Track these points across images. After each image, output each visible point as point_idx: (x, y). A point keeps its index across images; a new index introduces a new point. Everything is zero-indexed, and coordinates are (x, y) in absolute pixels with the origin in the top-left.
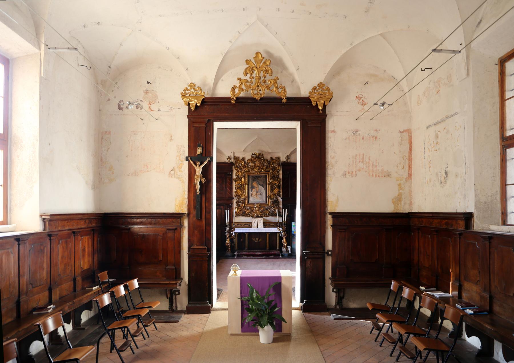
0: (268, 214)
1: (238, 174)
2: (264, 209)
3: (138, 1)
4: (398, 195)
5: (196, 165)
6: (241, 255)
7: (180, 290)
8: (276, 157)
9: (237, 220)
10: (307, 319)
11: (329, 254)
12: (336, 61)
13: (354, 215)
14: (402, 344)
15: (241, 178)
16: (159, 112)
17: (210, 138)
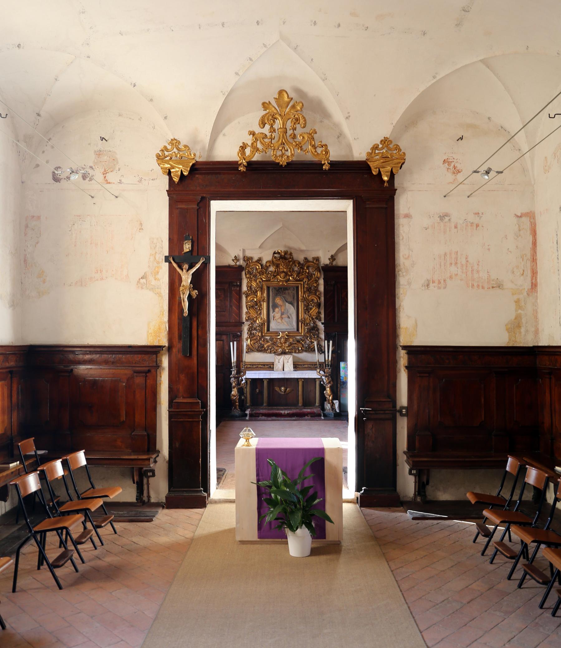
0: (300, 349)
1: (251, 285)
2: (293, 341)
3: (84, 11)
4: (516, 318)
5: (182, 270)
6: (258, 415)
7: (154, 470)
8: (313, 258)
9: (248, 358)
10: (368, 518)
11: (403, 413)
12: (409, 104)
13: (443, 349)
14: (528, 559)
15: (257, 292)
16: (120, 185)
17: (206, 226)
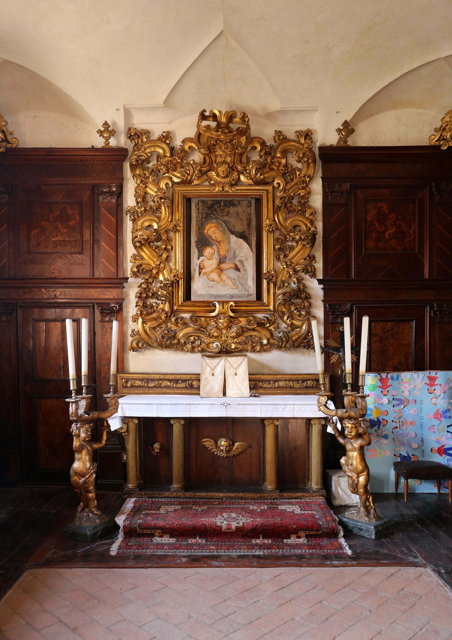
0: (265, 342)
8: (297, 132)
15: (159, 208)
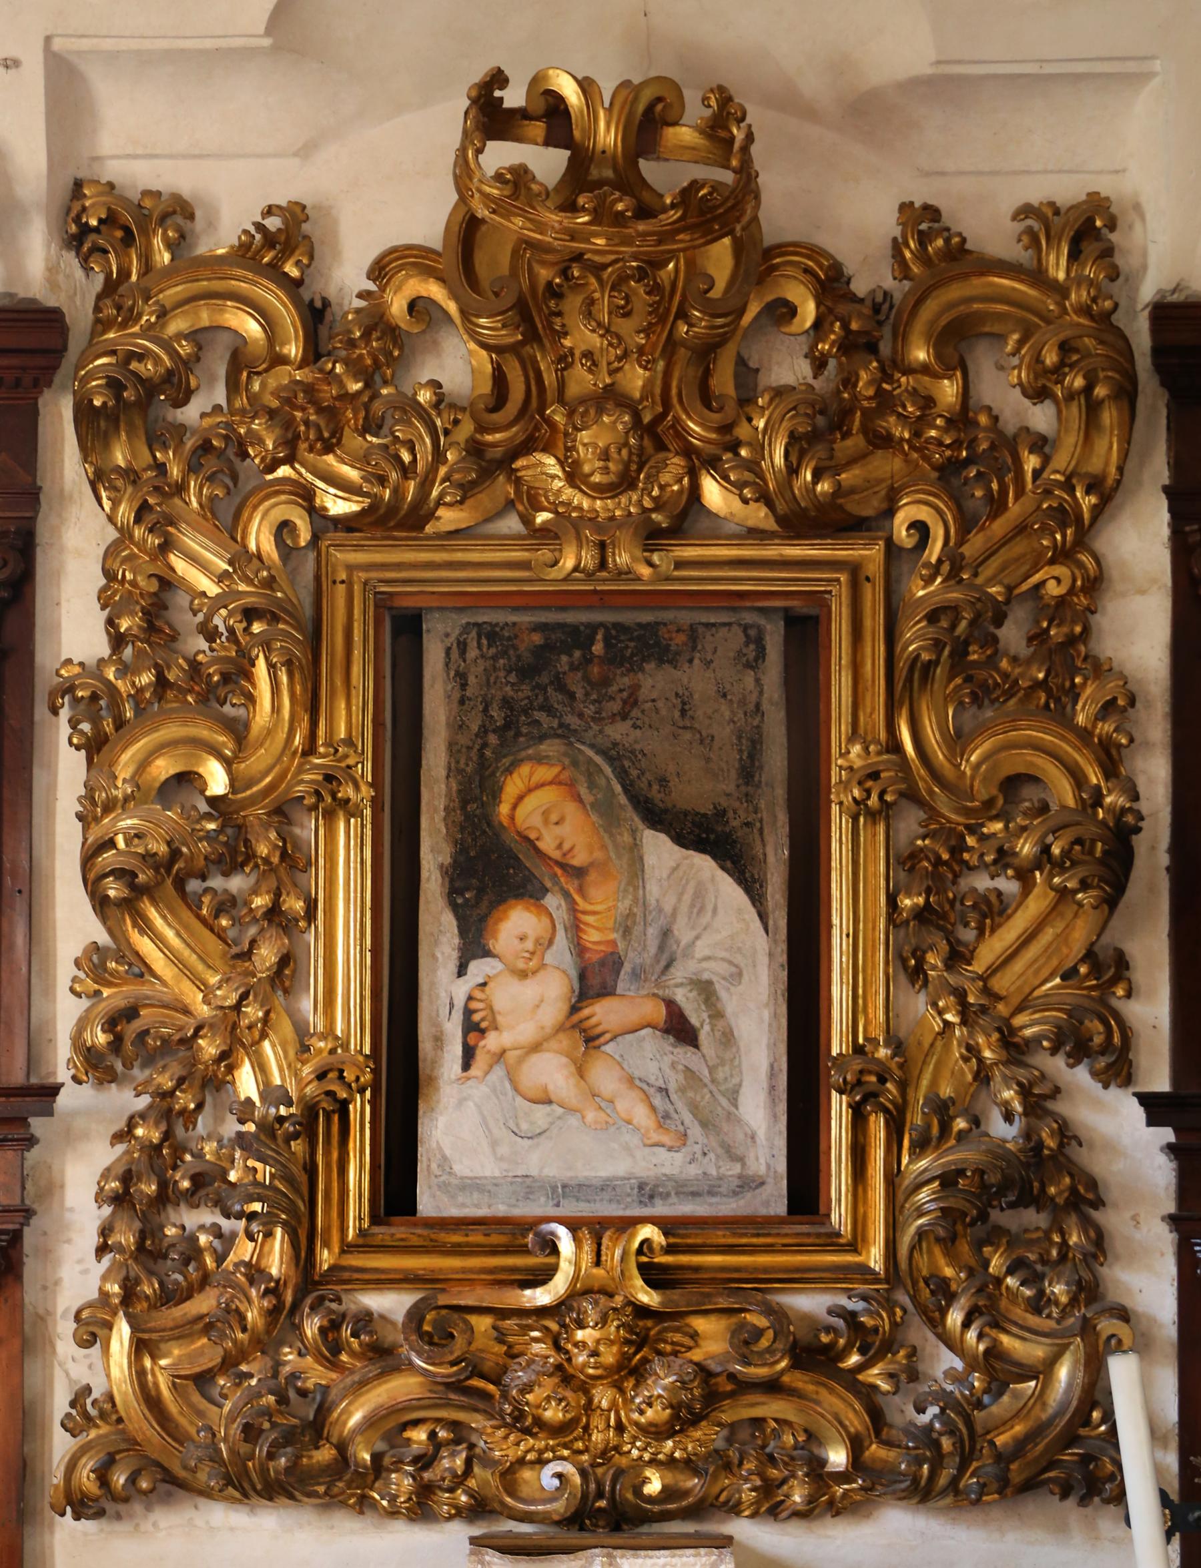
0: (838, 1457)
2: (745, 1341)
8: (1025, 211)
